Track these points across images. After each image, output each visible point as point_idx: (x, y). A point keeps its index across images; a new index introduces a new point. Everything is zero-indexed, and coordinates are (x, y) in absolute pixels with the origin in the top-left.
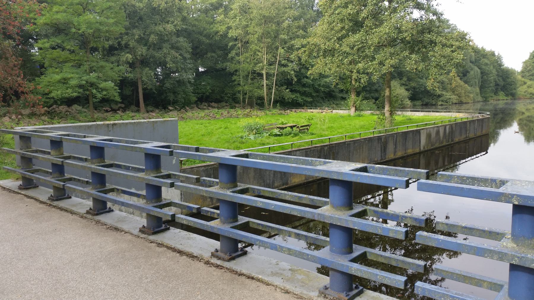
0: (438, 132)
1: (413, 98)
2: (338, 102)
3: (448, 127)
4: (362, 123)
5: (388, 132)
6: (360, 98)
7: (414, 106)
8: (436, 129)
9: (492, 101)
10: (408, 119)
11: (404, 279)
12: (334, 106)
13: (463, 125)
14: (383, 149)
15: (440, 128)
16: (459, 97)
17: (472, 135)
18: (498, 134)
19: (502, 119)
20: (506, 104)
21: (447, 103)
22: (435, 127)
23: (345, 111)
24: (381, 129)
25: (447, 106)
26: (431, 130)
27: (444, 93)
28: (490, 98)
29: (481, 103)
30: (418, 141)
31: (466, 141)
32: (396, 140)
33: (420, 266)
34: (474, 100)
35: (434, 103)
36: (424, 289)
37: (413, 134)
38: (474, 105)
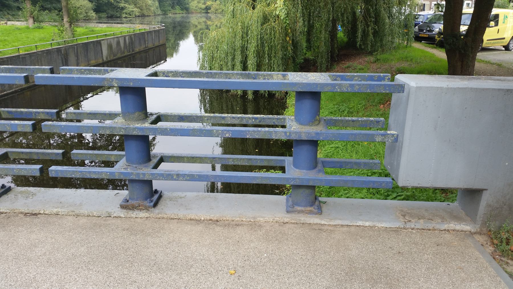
0: (118, 43)
1: (97, 10)
2: (14, 13)
3: (127, 38)
4: (42, 35)
5: (68, 43)
6: (37, 8)
7: (100, 18)
8: (116, 39)
9: (170, 15)
10: (90, 31)
11: (38, 167)
12: (10, 17)
13: (142, 36)
14: (64, 61)
15: (120, 38)
16: (141, 9)
17: (150, 45)
18: (178, 45)
19: (180, 31)
20: (183, 17)
21: (130, 15)
22: (115, 38)
23: (23, 23)
24: (60, 40)
25: (131, 18)
26: (112, 40)
27: (127, 5)
28: (168, 11)
29: (162, 16)
30: (100, 52)
31: (146, 51)
32: (77, 52)
33: (58, 154)
34: (155, 13)
35: (119, 15)
36: (56, 171)
37: (94, 44)
38: (155, 18)
